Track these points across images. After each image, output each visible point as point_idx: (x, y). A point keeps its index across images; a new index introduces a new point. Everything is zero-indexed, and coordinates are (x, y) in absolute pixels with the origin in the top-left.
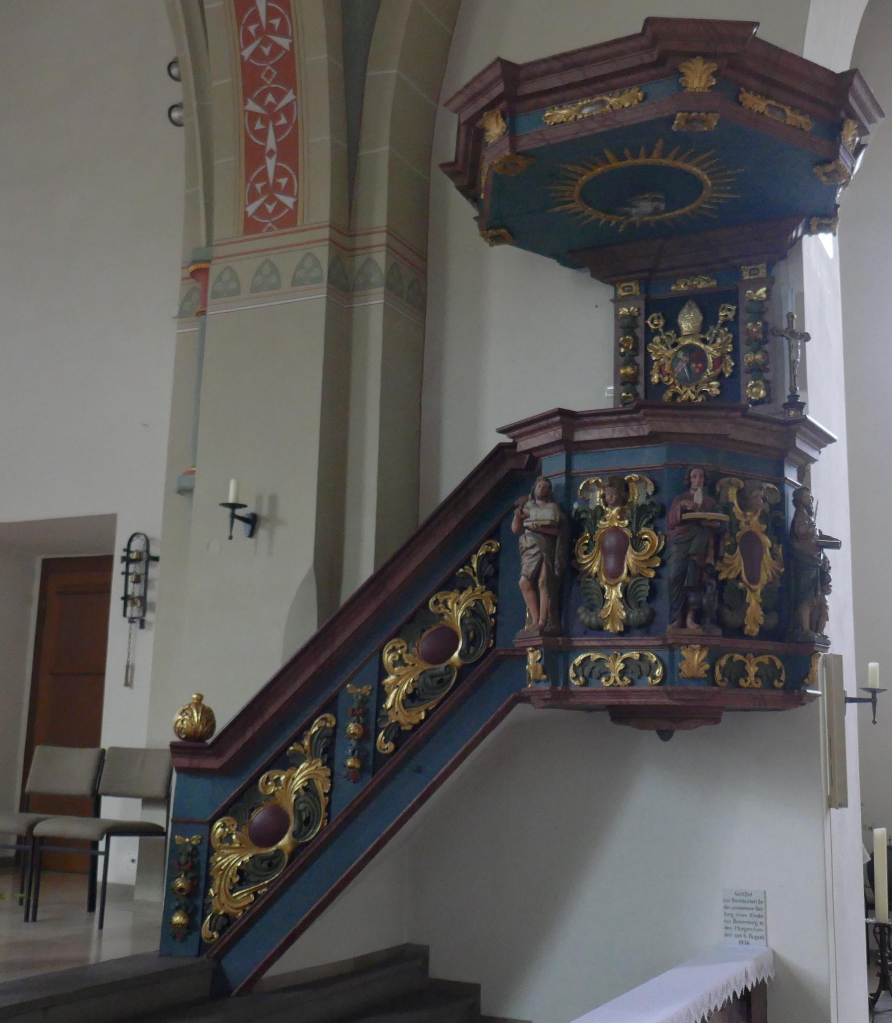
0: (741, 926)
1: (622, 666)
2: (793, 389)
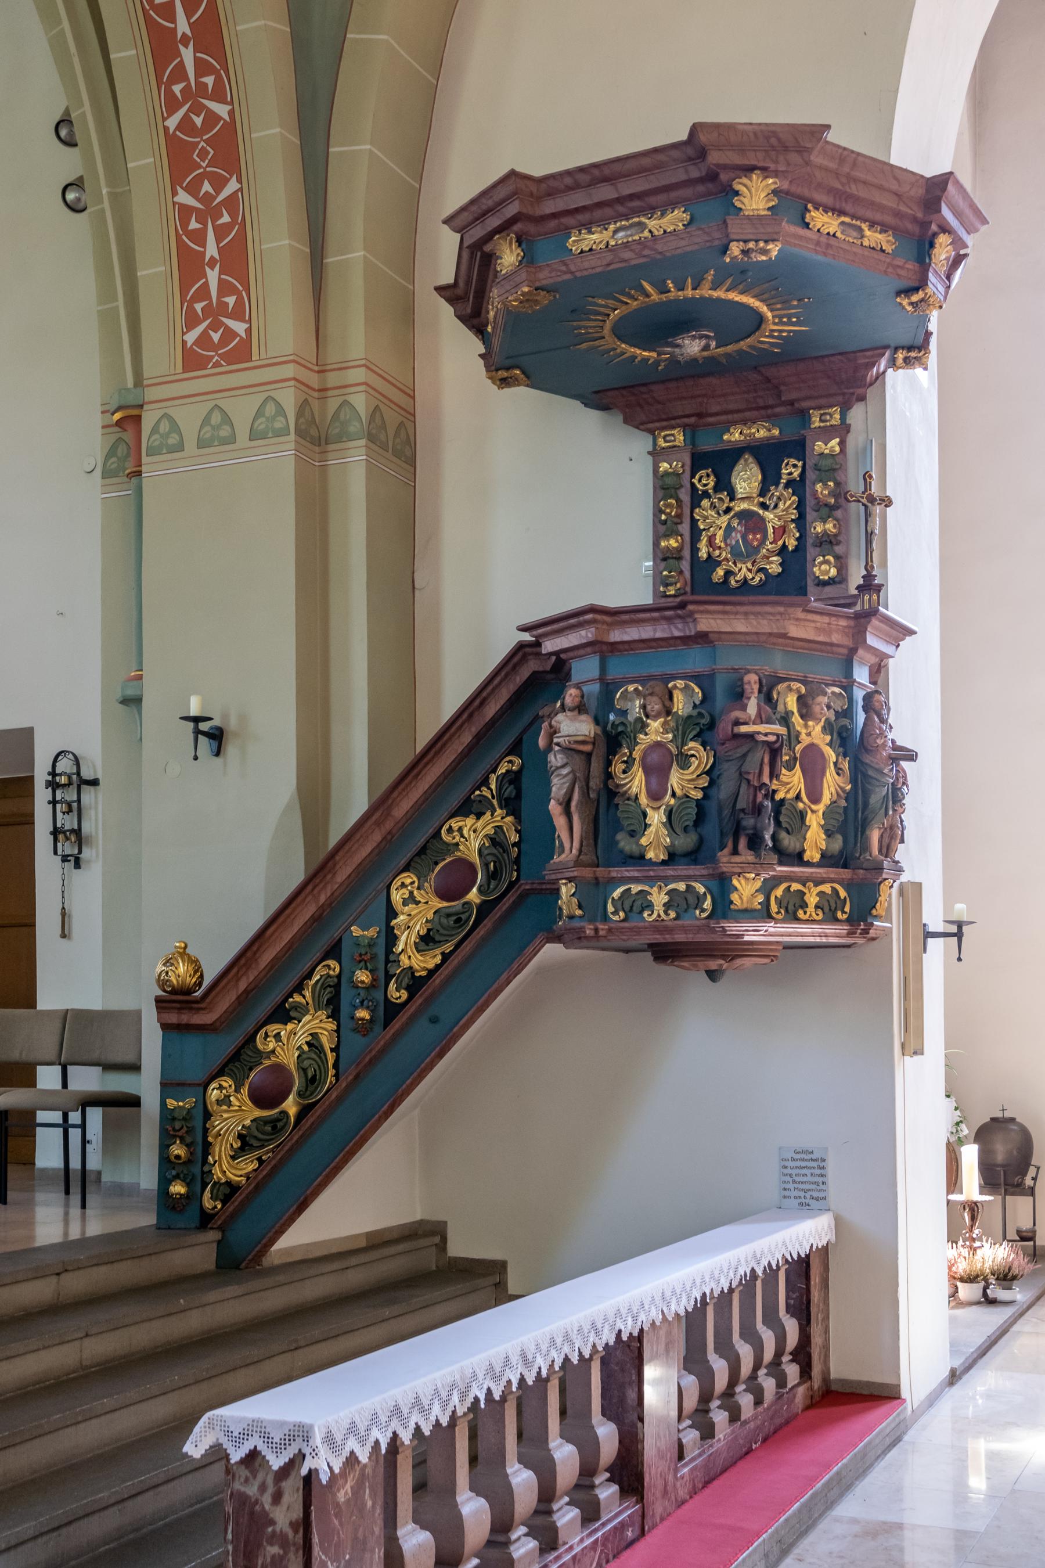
0: (801, 1186)
1: (666, 899)
2: (868, 567)
